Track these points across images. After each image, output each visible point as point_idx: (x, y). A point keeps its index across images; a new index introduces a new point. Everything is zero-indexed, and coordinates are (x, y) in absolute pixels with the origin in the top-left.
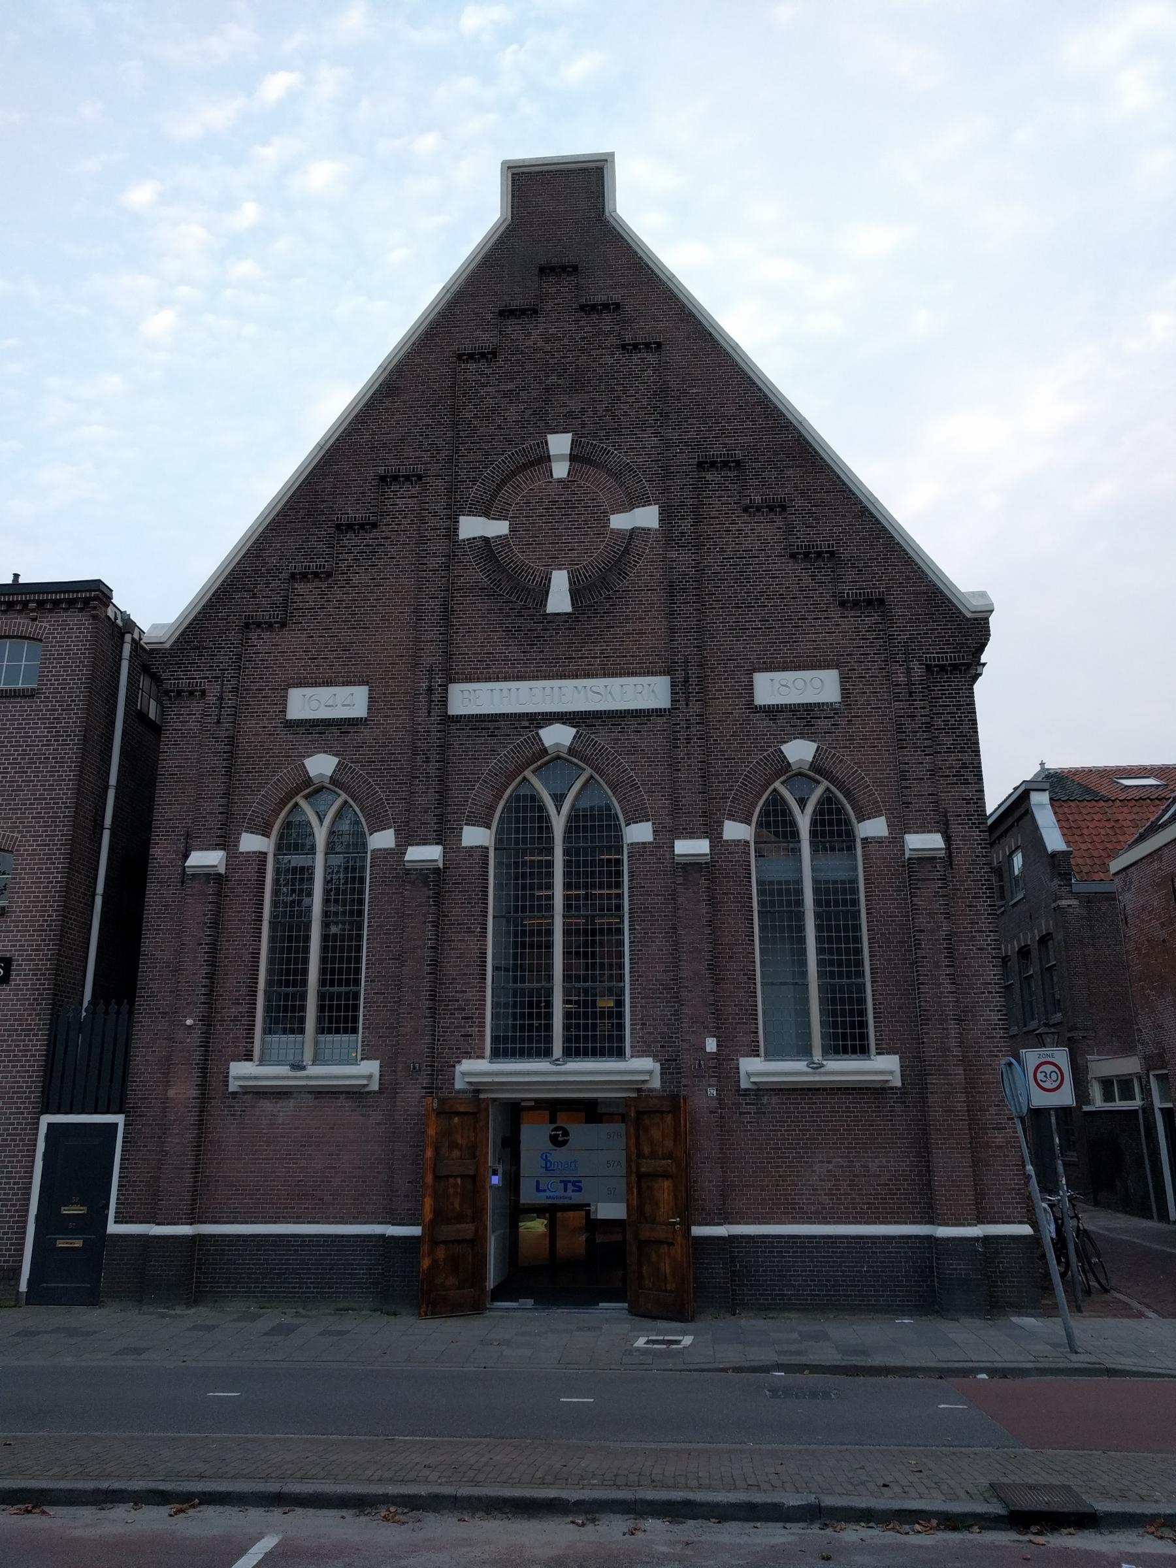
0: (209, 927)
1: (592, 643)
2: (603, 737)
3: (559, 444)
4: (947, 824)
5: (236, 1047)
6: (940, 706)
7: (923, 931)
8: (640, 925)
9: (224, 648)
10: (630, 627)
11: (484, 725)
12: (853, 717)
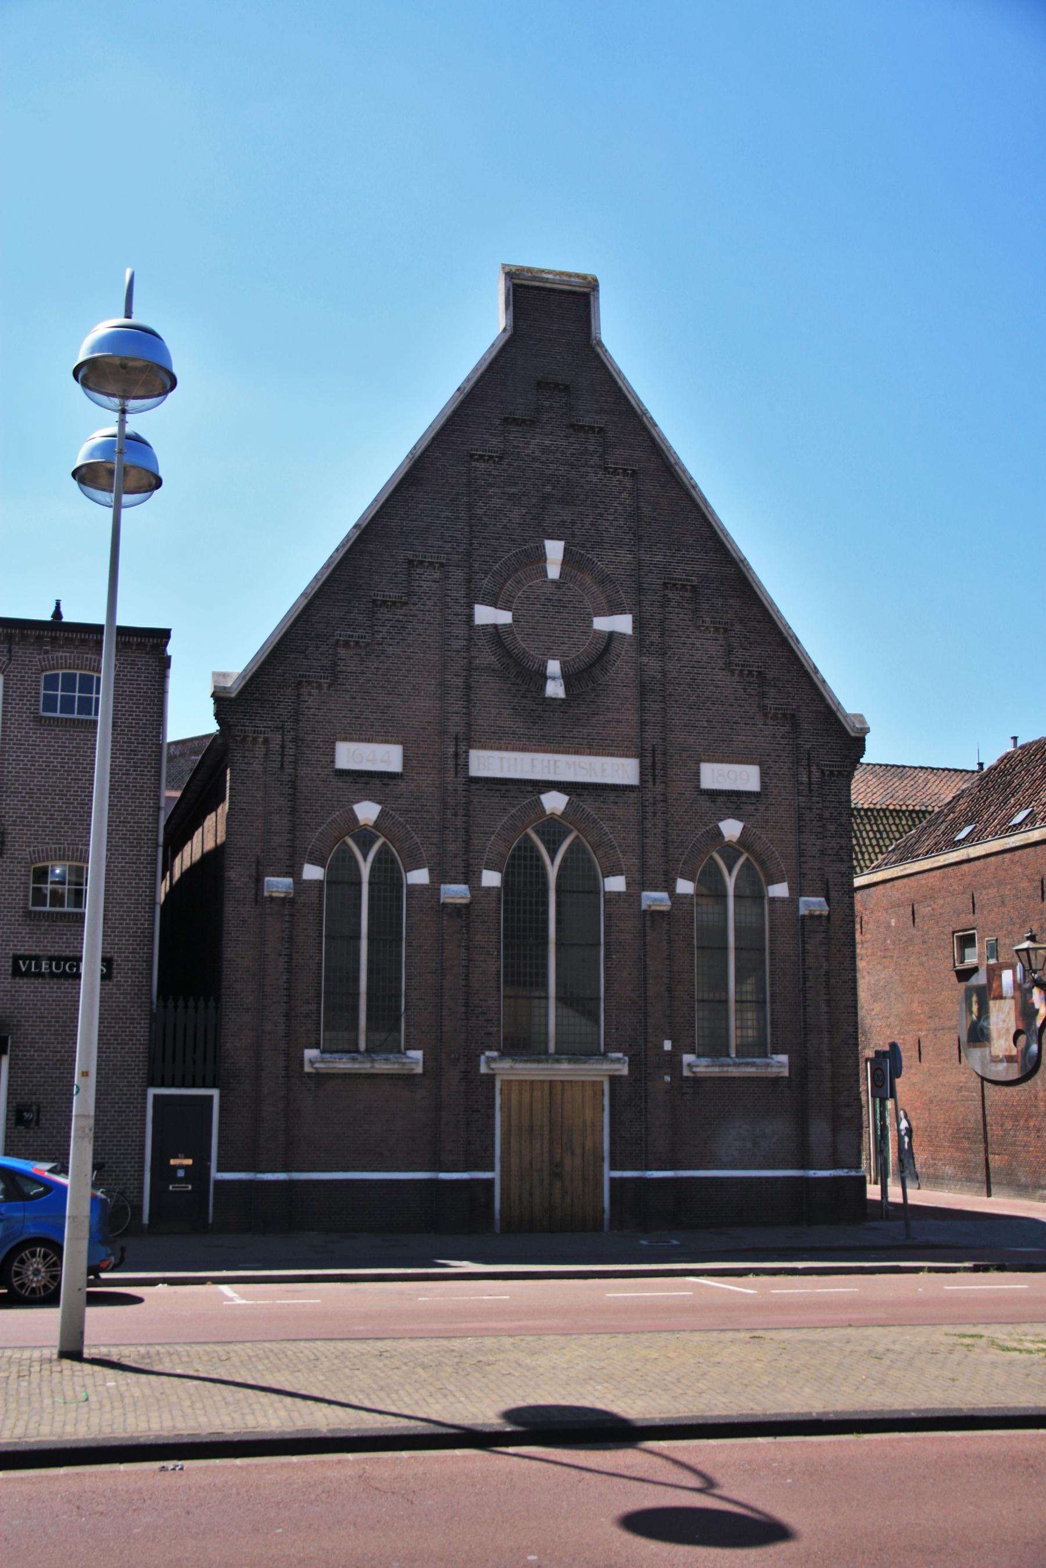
2: (589, 806)
3: (555, 550)
4: (828, 891)
7: (810, 968)
10: (610, 716)
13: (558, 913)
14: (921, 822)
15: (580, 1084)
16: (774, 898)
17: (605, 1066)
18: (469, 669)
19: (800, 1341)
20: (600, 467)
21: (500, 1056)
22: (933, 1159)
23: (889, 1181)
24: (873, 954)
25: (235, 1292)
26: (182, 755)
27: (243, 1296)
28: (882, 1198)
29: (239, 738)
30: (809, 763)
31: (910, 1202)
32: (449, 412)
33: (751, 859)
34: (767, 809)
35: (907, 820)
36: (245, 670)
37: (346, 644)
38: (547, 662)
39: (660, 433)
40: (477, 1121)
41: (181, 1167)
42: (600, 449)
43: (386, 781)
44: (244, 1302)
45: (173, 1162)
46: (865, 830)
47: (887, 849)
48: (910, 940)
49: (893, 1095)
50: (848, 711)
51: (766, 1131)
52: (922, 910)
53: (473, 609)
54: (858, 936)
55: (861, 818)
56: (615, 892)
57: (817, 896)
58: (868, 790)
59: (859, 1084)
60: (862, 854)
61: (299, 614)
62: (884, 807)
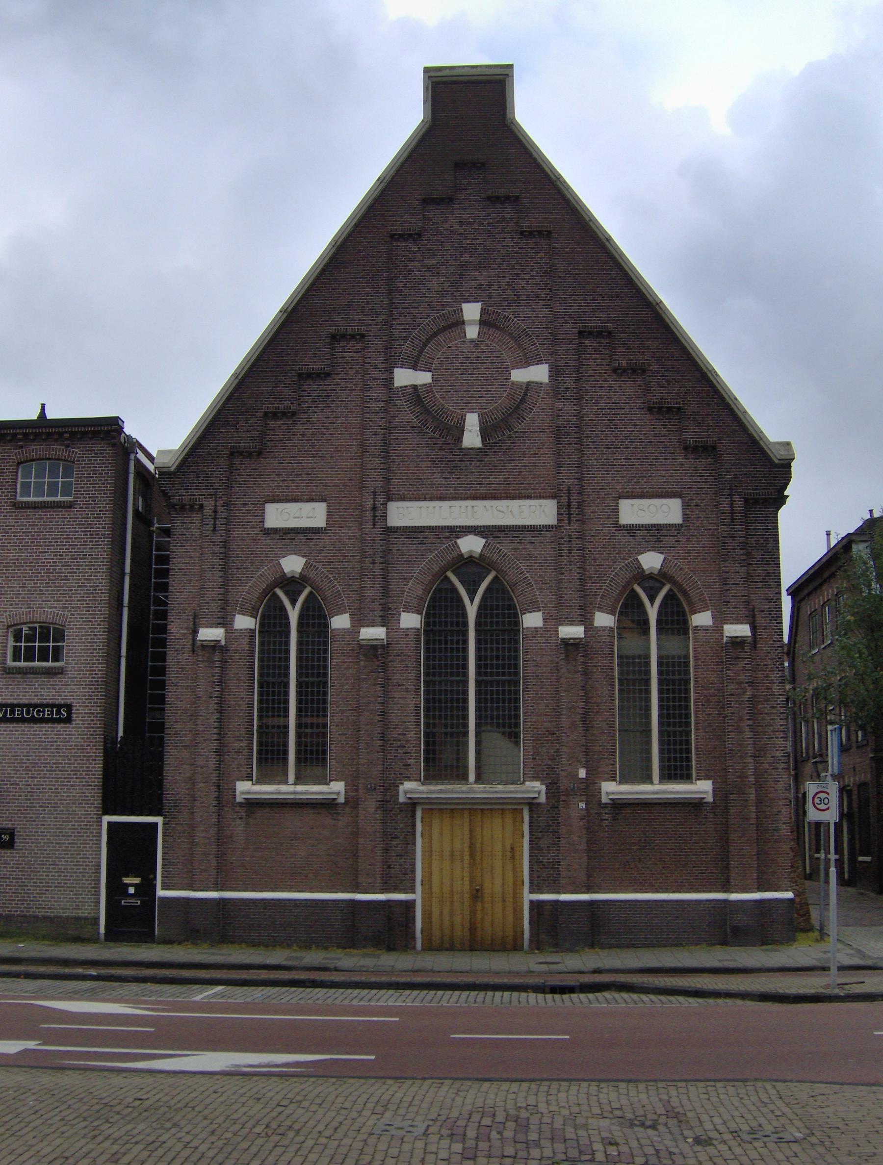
2: (506, 547)
3: (472, 311)
4: (754, 616)
10: (526, 461)
11: (415, 535)
29: (177, 507)
33: (675, 590)
34: (688, 540)
41: (131, 885)
43: (309, 536)
50: (772, 440)
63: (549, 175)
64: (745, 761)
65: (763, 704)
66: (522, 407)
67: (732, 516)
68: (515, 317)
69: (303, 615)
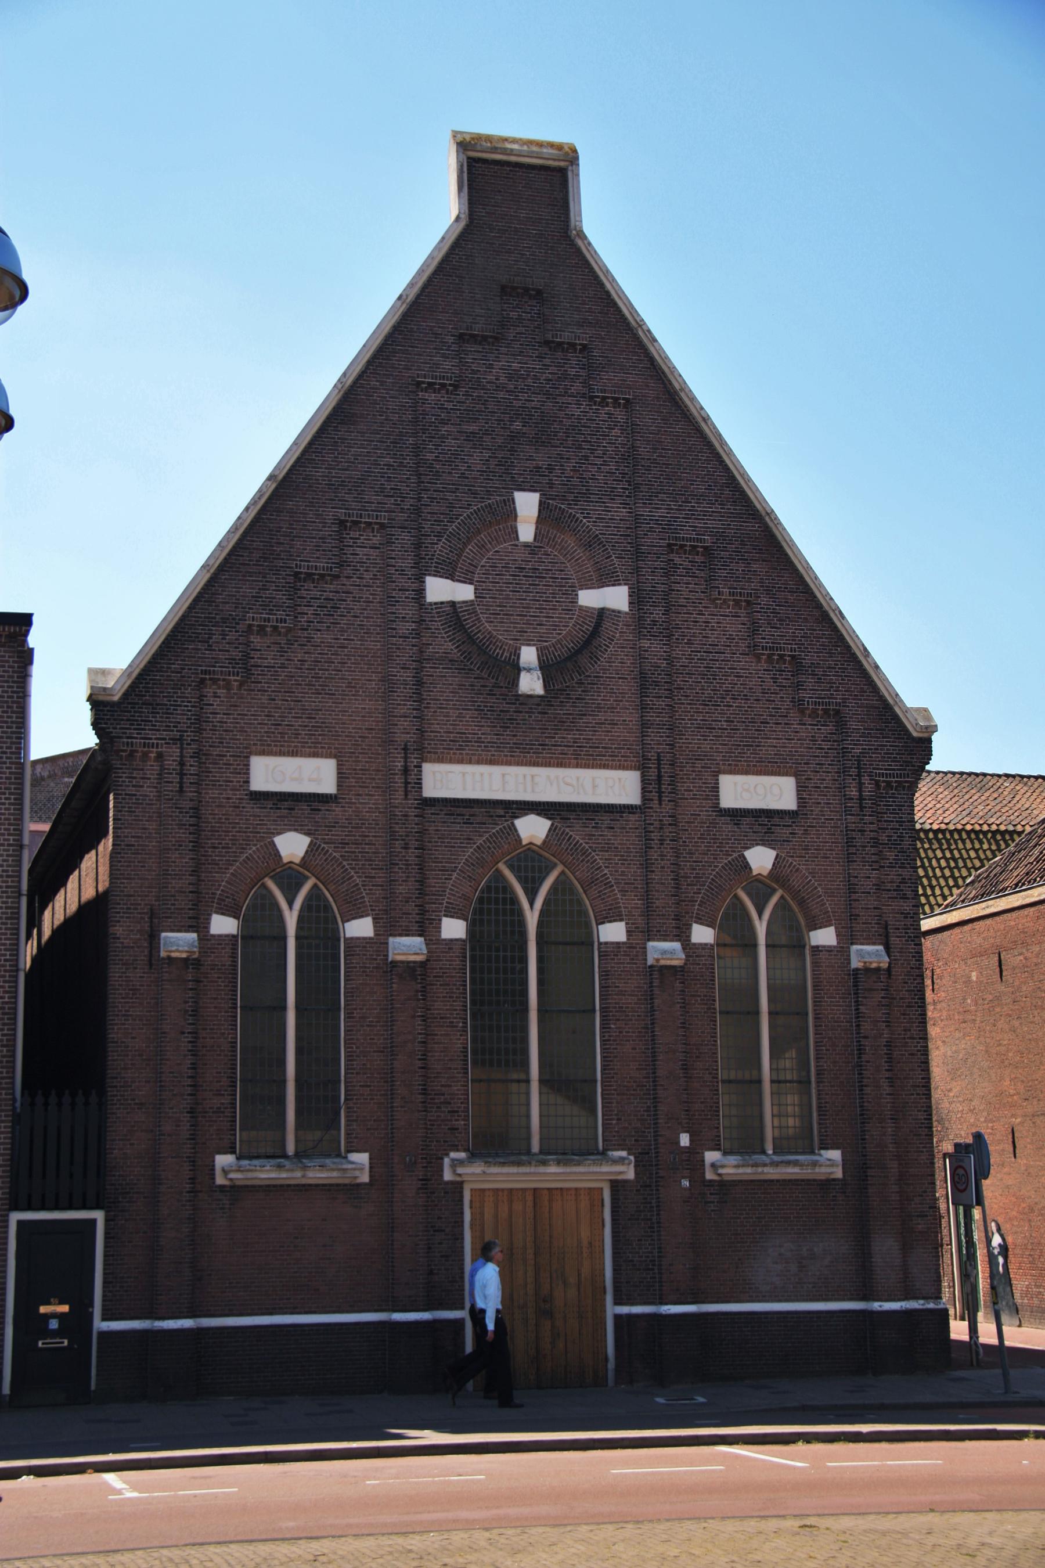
0: (191, 1015)
1: (565, 730)
2: (577, 833)
4: (887, 936)
5: (220, 1139)
6: (885, 821)
8: (615, 1024)
9: (180, 706)
10: (601, 717)
11: (459, 810)
12: (808, 826)
13: (540, 971)
14: (1007, 846)
15: (573, 1192)
16: (817, 947)
17: (605, 1169)
18: (420, 660)
19: (865, 1531)
20: (584, 396)
21: (469, 1158)
22: (1037, 1286)
23: (980, 1315)
24: (949, 1018)
25: (125, 1482)
26: (52, 776)
27: (134, 1487)
28: (971, 1338)
29: (124, 754)
30: (859, 772)
31: (1007, 1343)
32: (387, 329)
35: (990, 844)
36: (130, 666)
37: (262, 629)
38: (520, 649)
39: (660, 350)
40: (440, 1243)
41: (54, 1315)
42: (583, 373)
44: (135, 1494)
45: (43, 1309)
46: (935, 857)
47: (964, 882)
48: (998, 998)
49: (980, 1202)
51: (816, 1249)
52: (1012, 960)
53: (424, 582)
54: (929, 995)
55: (930, 841)
56: (612, 943)
57: (874, 944)
58: (938, 806)
59: (934, 1188)
60: (932, 888)
61: (199, 593)
62: (959, 827)
63: (626, 319)
64: (883, 1125)
65: (900, 1051)
66: (595, 643)
67: (861, 804)
68: (584, 517)
69: (543, 921)
